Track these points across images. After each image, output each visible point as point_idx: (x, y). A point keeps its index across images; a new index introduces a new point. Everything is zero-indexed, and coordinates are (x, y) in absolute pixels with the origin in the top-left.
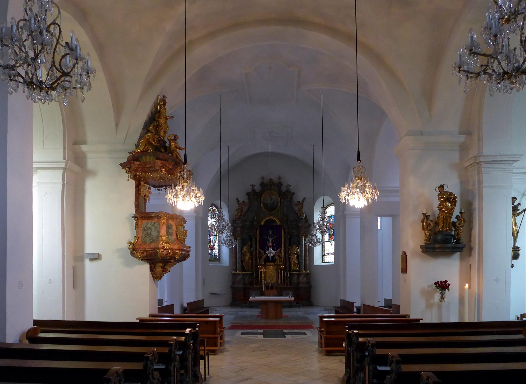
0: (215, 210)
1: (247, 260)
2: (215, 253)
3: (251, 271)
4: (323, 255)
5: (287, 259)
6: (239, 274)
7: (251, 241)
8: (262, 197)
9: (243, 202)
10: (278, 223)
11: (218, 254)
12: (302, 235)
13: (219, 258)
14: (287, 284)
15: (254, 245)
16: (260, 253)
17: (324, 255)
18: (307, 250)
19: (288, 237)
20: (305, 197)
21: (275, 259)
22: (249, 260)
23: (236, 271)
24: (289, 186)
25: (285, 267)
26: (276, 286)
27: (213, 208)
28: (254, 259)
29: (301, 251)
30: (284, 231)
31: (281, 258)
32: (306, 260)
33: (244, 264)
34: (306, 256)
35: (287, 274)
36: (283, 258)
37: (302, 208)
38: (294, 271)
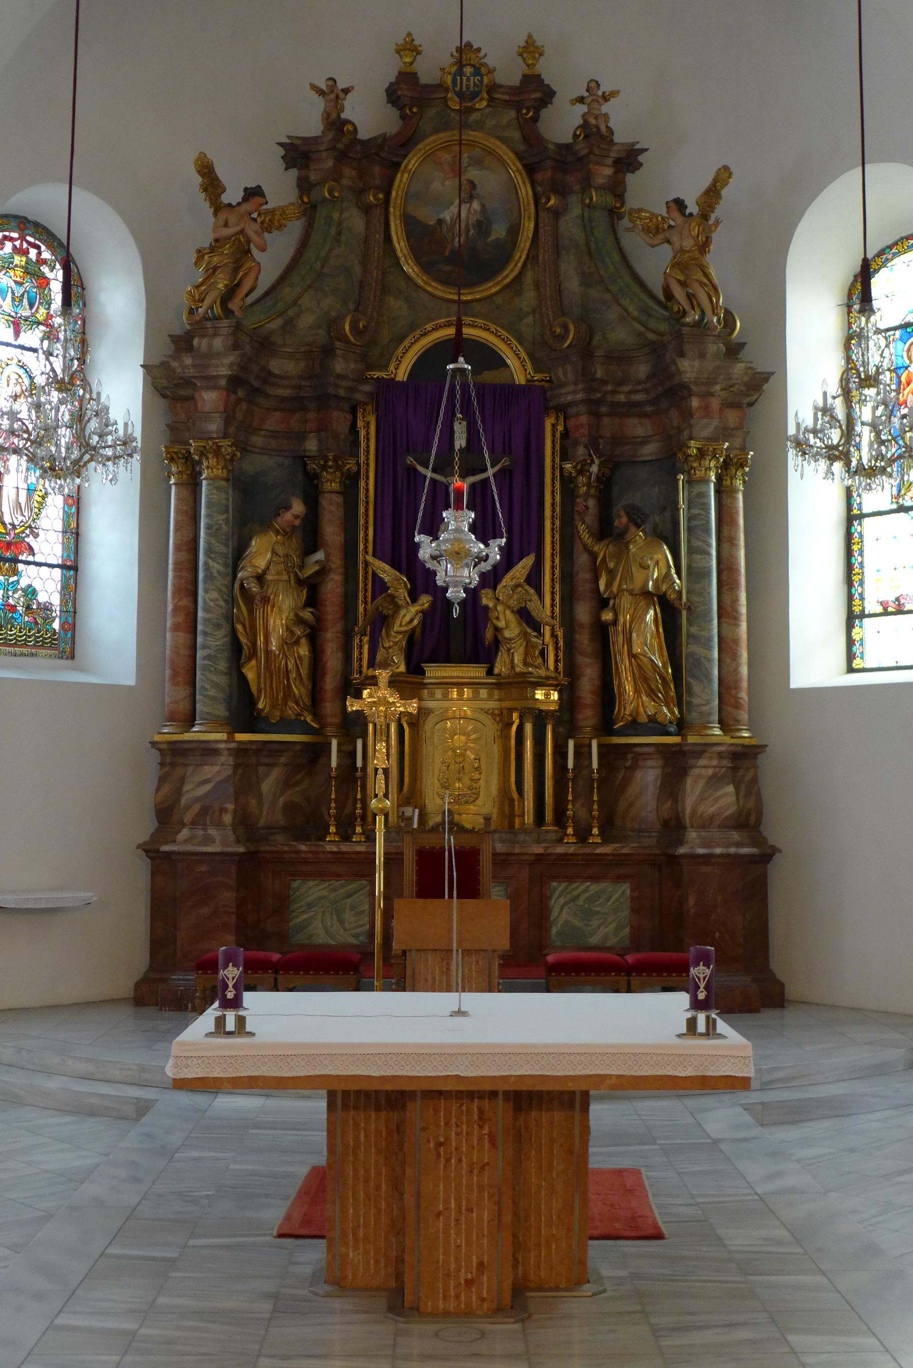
0: (45, 269)
1: (274, 647)
2: (37, 585)
3: (308, 730)
4: (853, 617)
5: (584, 639)
6: (207, 751)
7: (312, 499)
8: (402, 179)
9: (253, 193)
10: (511, 361)
11: (56, 600)
12: (702, 453)
13: (71, 625)
14: (583, 836)
15: (332, 532)
16: (380, 586)
17: (863, 615)
18: (737, 571)
19: (594, 469)
20: (726, 168)
21: (489, 634)
22: (289, 643)
23: (190, 720)
24: (606, 98)
25: (569, 700)
26: (500, 848)
27: (33, 253)
28: (331, 637)
29: (697, 576)
30: (565, 435)
31: (540, 634)
32: (727, 646)
33: (250, 673)
34: (727, 613)
35: (582, 753)
36: (554, 635)
37: (704, 247)
38: (634, 727)
